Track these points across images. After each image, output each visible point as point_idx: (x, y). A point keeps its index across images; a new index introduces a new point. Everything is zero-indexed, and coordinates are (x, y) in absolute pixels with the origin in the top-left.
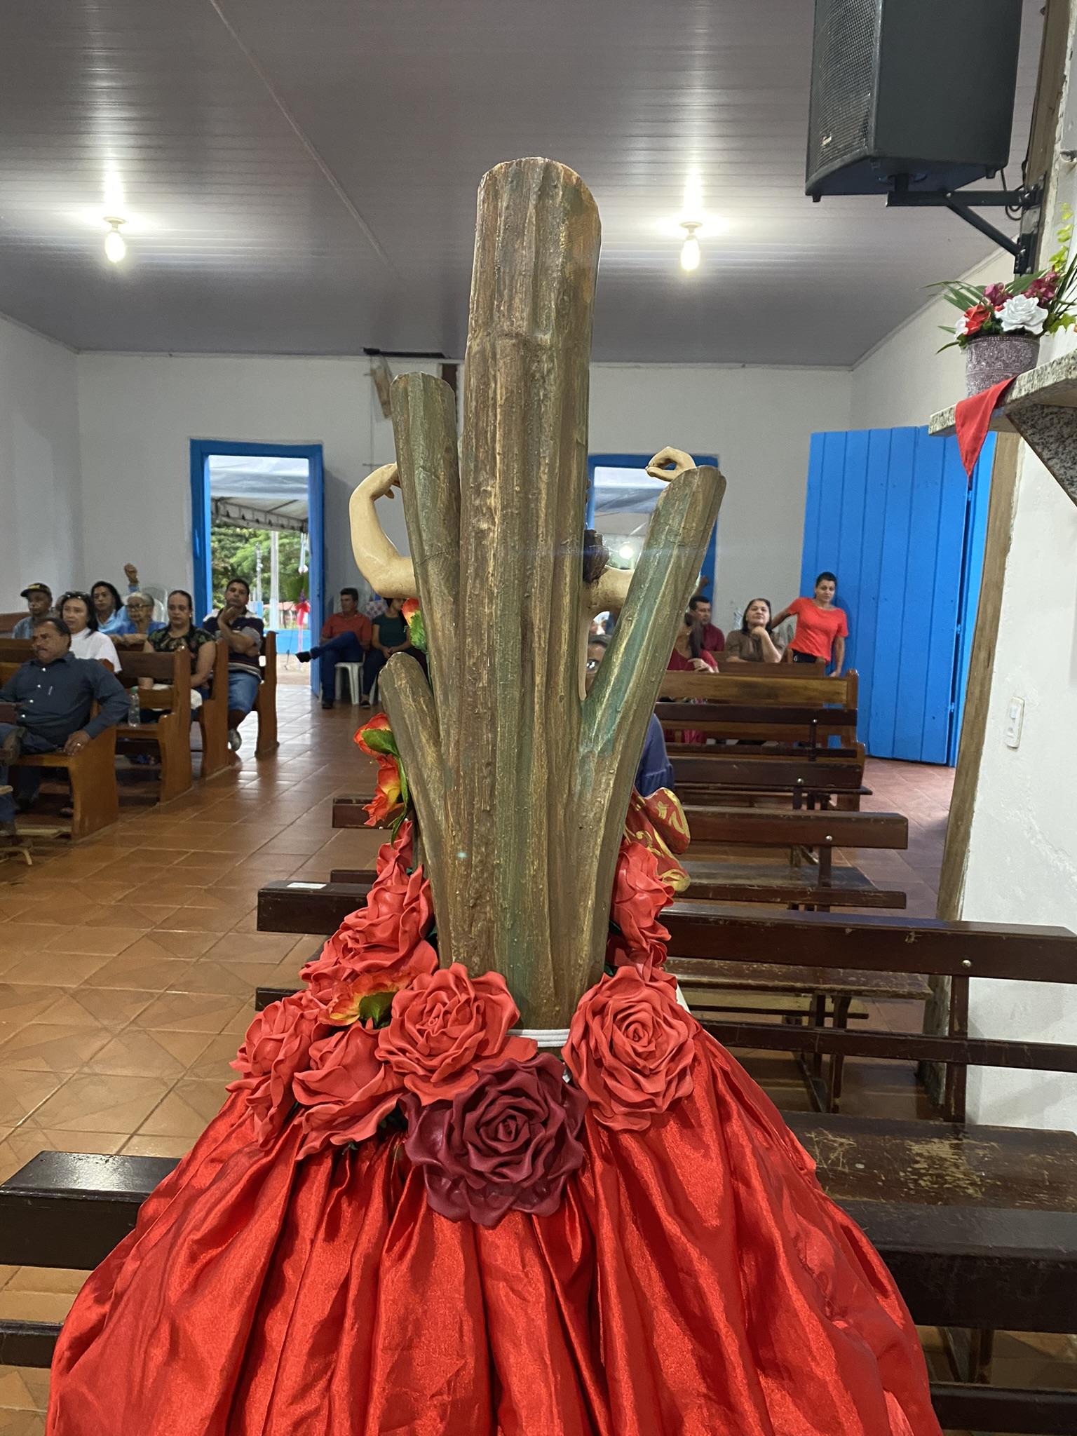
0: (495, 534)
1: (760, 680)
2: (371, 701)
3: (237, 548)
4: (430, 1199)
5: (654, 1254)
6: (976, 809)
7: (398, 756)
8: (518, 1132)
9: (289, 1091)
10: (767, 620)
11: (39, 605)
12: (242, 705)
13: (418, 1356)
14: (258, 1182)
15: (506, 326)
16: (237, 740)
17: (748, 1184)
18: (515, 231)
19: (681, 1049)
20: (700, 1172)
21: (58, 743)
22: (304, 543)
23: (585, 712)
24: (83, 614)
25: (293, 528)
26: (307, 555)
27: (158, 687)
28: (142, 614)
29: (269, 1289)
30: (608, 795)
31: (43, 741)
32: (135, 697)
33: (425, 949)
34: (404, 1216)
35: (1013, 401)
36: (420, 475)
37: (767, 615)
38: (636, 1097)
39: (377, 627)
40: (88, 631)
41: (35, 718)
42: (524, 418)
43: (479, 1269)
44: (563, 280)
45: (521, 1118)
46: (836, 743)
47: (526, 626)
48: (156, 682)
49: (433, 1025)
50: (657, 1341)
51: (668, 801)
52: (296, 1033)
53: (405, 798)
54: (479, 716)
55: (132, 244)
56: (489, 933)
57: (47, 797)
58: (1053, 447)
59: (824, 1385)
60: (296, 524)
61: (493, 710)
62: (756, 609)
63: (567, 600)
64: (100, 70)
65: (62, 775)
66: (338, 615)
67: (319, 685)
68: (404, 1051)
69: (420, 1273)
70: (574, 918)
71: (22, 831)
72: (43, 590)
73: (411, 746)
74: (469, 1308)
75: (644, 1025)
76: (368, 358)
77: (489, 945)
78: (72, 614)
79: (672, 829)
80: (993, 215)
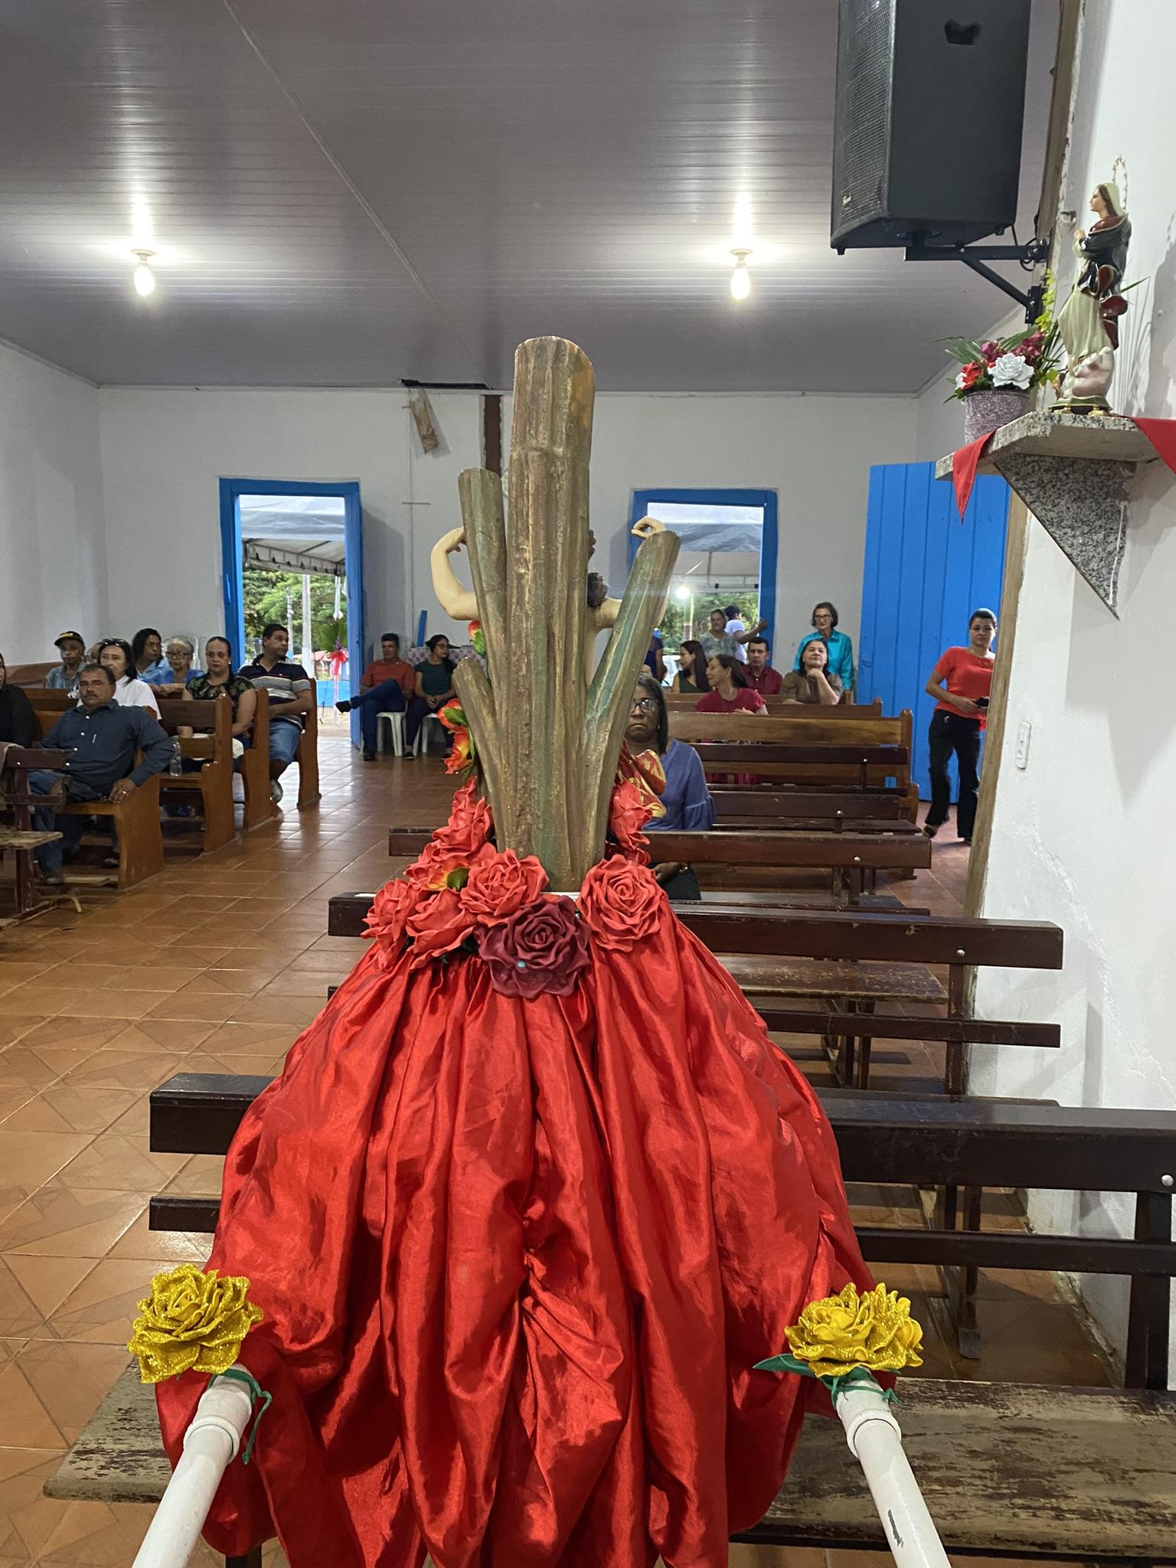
0: (529, 577)
1: (813, 721)
2: (415, 753)
3: (264, 594)
4: (494, 984)
5: (633, 1022)
6: (993, 828)
7: (468, 725)
8: (547, 938)
9: (404, 932)
10: (824, 662)
11: (73, 654)
12: (284, 754)
13: (489, 1070)
14: (384, 988)
15: (534, 443)
16: (278, 792)
17: (694, 986)
18: (539, 383)
19: (650, 903)
20: (663, 974)
21: (103, 791)
22: (340, 587)
23: (590, 692)
24: (122, 661)
25: (326, 571)
26: (343, 599)
27: (198, 736)
28: (183, 662)
29: (395, 1045)
30: (605, 745)
31: (89, 789)
32: (177, 745)
33: (489, 846)
34: (479, 996)
35: (995, 452)
36: (480, 538)
37: (824, 656)
38: (622, 927)
39: (420, 675)
40: (127, 678)
41: (77, 767)
42: (547, 502)
43: (524, 1025)
44: (570, 414)
45: (549, 930)
46: (891, 783)
47: (550, 635)
48: (195, 731)
49: (495, 883)
50: (634, 1073)
51: (651, 758)
52: (407, 897)
53: (473, 753)
54: (520, 694)
55: (160, 275)
56: (529, 832)
57: (87, 849)
58: (1035, 491)
59: (736, 1096)
60: (330, 567)
61: (530, 690)
62: (813, 650)
63: (576, 619)
64: (128, 107)
65: (107, 825)
66: (379, 663)
67: (360, 736)
68: (475, 899)
69: (489, 1026)
70: (583, 823)
71: (70, 879)
72: (76, 637)
73: (476, 718)
74: (519, 1046)
75: (627, 887)
76: (406, 389)
77: (529, 839)
78: (111, 662)
79: (654, 777)
80: (1008, 270)
